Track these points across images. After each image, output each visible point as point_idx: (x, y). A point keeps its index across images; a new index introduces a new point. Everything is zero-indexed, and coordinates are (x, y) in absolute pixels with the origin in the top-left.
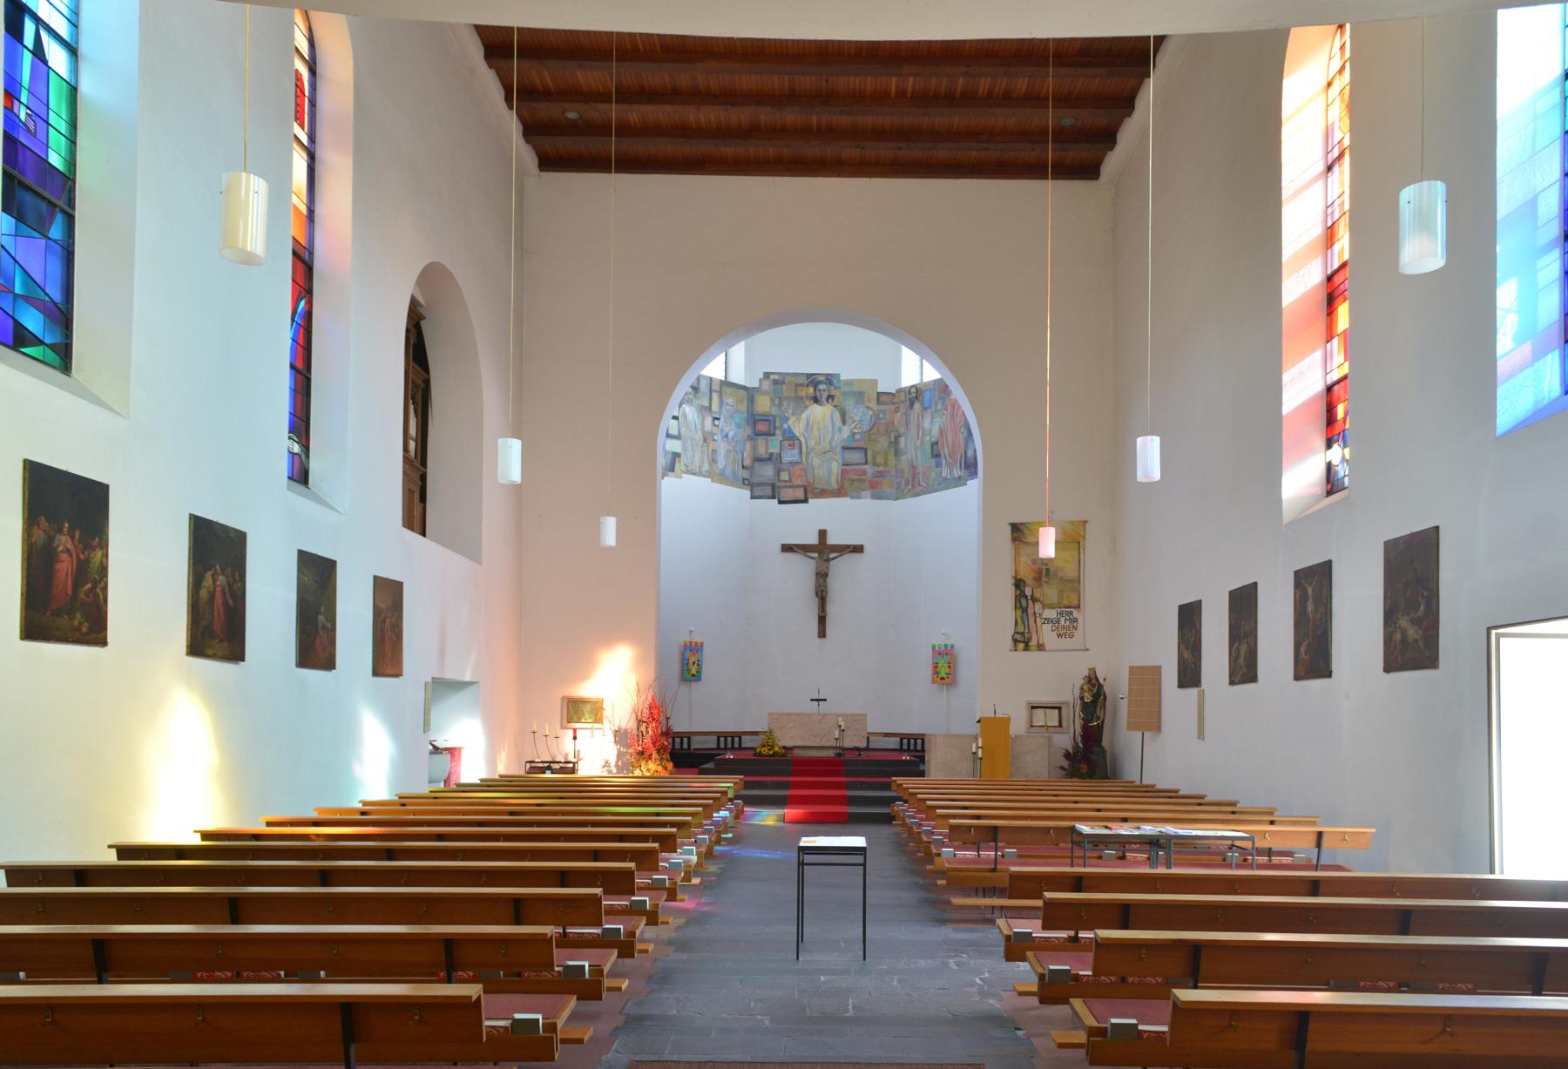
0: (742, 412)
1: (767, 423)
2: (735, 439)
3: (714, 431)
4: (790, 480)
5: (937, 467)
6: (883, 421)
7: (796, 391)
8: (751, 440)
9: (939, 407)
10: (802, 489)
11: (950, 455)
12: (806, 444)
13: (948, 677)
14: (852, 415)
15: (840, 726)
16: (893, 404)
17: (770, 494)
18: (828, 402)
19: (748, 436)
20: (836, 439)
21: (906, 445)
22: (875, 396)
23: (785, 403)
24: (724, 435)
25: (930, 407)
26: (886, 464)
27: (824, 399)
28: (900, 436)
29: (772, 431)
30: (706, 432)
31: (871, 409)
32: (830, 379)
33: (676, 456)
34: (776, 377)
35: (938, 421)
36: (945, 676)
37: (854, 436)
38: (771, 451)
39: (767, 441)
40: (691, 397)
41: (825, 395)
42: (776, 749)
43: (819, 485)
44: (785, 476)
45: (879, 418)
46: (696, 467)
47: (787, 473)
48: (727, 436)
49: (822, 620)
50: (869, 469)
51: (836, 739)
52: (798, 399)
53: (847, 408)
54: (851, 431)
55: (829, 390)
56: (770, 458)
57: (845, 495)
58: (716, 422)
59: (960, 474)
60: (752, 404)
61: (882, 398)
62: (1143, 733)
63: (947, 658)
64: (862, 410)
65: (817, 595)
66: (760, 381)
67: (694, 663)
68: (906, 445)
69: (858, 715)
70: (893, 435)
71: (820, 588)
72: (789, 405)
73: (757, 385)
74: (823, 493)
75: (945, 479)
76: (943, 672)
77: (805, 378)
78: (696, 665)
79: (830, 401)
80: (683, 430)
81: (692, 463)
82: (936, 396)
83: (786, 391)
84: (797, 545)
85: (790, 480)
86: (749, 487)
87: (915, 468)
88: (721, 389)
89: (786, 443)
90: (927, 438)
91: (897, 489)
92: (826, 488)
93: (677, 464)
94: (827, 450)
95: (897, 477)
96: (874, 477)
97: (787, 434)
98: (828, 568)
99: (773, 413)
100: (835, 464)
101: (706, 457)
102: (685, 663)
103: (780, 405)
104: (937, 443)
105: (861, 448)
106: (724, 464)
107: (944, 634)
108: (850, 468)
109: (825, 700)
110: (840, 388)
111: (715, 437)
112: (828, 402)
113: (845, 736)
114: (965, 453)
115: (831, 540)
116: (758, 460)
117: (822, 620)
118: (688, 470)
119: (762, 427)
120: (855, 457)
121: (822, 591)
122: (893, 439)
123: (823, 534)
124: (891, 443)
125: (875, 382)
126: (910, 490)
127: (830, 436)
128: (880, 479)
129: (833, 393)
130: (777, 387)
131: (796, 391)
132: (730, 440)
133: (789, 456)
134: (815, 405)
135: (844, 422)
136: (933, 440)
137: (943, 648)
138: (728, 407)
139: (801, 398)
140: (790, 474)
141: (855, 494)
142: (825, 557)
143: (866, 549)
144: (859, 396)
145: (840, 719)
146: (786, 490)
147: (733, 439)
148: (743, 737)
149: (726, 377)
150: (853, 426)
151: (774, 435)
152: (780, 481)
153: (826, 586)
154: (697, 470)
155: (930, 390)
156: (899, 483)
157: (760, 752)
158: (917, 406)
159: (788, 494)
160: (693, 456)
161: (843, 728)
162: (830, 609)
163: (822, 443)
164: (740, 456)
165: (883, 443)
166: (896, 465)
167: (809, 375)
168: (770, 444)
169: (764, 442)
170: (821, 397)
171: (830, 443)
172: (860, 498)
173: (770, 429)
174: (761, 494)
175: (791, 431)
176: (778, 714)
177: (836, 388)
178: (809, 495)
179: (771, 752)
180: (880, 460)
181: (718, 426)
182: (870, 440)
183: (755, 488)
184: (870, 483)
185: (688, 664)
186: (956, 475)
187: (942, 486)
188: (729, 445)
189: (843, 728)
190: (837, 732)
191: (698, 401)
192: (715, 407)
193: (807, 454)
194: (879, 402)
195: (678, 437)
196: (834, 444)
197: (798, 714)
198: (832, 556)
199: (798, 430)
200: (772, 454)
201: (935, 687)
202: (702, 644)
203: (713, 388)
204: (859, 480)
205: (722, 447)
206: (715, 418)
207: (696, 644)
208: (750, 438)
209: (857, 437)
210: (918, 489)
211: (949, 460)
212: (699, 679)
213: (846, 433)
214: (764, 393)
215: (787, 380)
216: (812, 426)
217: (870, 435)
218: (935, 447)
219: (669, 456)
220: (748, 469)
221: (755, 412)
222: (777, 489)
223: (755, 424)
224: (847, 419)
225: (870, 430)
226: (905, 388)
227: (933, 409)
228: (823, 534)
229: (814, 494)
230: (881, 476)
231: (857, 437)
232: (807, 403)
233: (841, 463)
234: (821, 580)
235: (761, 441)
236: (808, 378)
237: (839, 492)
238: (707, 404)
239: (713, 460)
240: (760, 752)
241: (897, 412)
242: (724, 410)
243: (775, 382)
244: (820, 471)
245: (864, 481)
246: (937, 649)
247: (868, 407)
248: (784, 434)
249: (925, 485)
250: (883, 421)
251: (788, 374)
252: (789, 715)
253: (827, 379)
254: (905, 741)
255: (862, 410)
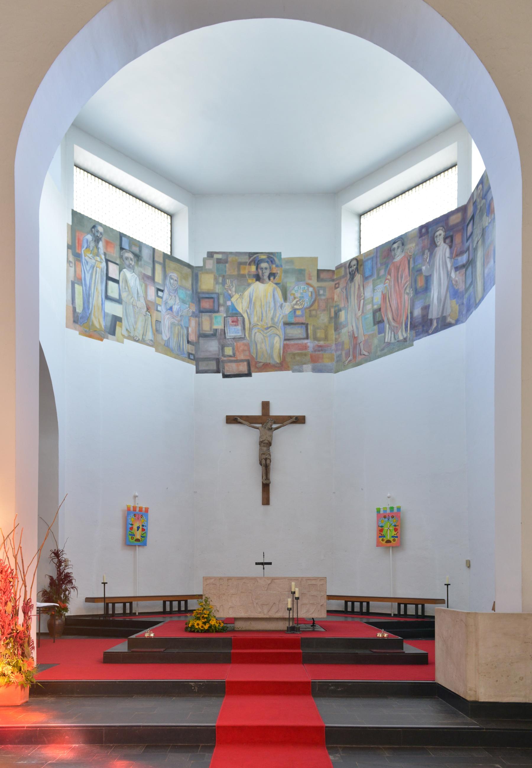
0: (186, 289)
1: (212, 300)
2: (180, 314)
3: (157, 302)
4: (234, 355)
5: (380, 333)
6: (323, 297)
7: (239, 270)
8: (196, 317)
9: (382, 272)
10: (246, 363)
11: (393, 319)
12: (249, 319)
13: (394, 540)
14: (293, 292)
15: (294, 593)
16: (333, 280)
17: (215, 368)
18: (269, 279)
19: (193, 313)
20: (278, 315)
21: (346, 318)
22: (315, 273)
23: (228, 281)
24: (168, 307)
25: (371, 276)
26: (326, 338)
27: (266, 277)
28: (340, 310)
29: (216, 309)
30: (149, 301)
31: (312, 286)
32: (271, 257)
33: (116, 320)
34: (220, 256)
35: (380, 288)
36: (392, 539)
37: (295, 312)
38: (215, 327)
39: (211, 319)
40: (133, 263)
41: (267, 274)
42: (213, 622)
43: (262, 360)
44: (228, 351)
45: (320, 295)
46: (139, 333)
47: (231, 348)
48: (171, 309)
49: (266, 487)
50: (310, 343)
51: (289, 609)
52: (241, 277)
53: (288, 285)
54: (293, 307)
55: (270, 268)
56: (214, 334)
57: (287, 369)
58: (160, 293)
59: (405, 335)
60: (197, 282)
61: (322, 276)
62: (264, 576)
63: (394, 521)
64: (302, 287)
65: (261, 464)
66: (204, 260)
67: (138, 528)
68: (346, 318)
69: (316, 579)
70: (333, 311)
71: (264, 456)
72: (232, 282)
73: (201, 264)
74: (266, 367)
75: (389, 344)
76: (389, 534)
77: (247, 257)
78: (140, 529)
79: (272, 278)
80: (124, 295)
81: (134, 330)
82: (378, 263)
83: (230, 269)
84: (241, 417)
85: (234, 355)
86: (194, 362)
87: (355, 338)
88: (164, 261)
89: (230, 320)
90: (369, 307)
91: (337, 361)
92: (268, 362)
93: (118, 329)
94: (269, 326)
95: (337, 350)
96: (315, 351)
97: (230, 311)
98: (271, 436)
99: (217, 291)
100: (277, 339)
101: (150, 326)
102: (129, 529)
103: (224, 283)
104: (380, 310)
105: (302, 324)
106: (168, 336)
107: (389, 497)
108: (292, 342)
109: (270, 564)
110: (281, 266)
111: (159, 308)
112: (269, 279)
113: (299, 605)
114: (412, 313)
115: (274, 412)
116: (203, 336)
117: (266, 487)
118: (129, 336)
119: (206, 304)
120: (297, 332)
121: (266, 459)
122: (333, 314)
123: (266, 405)
124: (331, 318)
125: (314, 260)
126: (350, 361)
127: (272, 312)
128: (321, 353)
129: (274, 272)
130: (221, 266)
131: (239, 270)
132: (175, 314)
133: (233, 332)
134: (258, 282)
135: (285, 299)
136: (376, 307)
137: (388, 511)
138: (172, 281)
139: (243, 276)
140: (233, 349)
141: (296, 367)
142: (268, 426)
143: (307, 420)
144: (300, 274)
145: (293, 584)
146: (229, 364)
147: (178, 312)
148: (189, 601)
149: (171, 252)
150: (294, 302)
151: (218, 312)
152: (224, 355)
153: (270, 455)
154: (141, 338)
155: (372, 258)
156: (339, 356)
157: (193, 626)
158: (358, 278)
159: (231, 368)
160: (136, 323)
161: (297, 595)
162: (275, 478)
163: (264, 318)
164: (185, 331)
165: (324, 318)
166: (336, 339)
167: (251, 254)
168: (214, 321)
169: (208, 318)
170: (263, 275)
171: (272, 319)
172: (300, 371)
173: (214, 306)
174: (207, 368)
175: (234, 308)
176: (215, 578)
177: (277, 266)
178: (252, 369)
179: (206, 627)
180: (320, 334)
181: (161, 298)
182: (311, 316)
183: (200, 363)
184: (311, 357)
185: (131, 529)
186: (401, 338)
187: (385, 351)
188: (173, 318)
189: (297, 595)
190: (290, 600)
191: (140, 269)
192: (159, 277)
193: (250, 330)
194: (319, 279)
195: (119, 301)
196: (276, 320)
197: (241, 578)
198: (274, 426)
199: (241, 306)
200: (216, 330)
201: (379, 550)
202: (147, 510)
203: (156, 259)
204: (299, 355)
205: (167, 321)
206: (158, 290)
207: (141, 509)
208: (194, 315)
209: (299, 313)
210: (359, 358)
211: (393, 323)
212: (144, 544)
213: (287, 309)
214: (208, 272)
215: (229, 260)
216: (254, 303)
217: (310, 311)
218: (378, 314)
219: (109, 319)
220: (193, 345)
221: (199, 290)
222: (221, 364)
223: (199, 301)
224: (289, 295)
225: (311, 306)
226: (345, 263)
227: (375, 277)
228: (266, 405)
229: (256, 367)
230: (322, 350)
231: (299, 313)
232: (250, 281)
233: (282, 337)
234: (265, 449)
235: (205, 318)
236: (250, 257)
237: (282, 366)
238: (149, 273)
239: (157, 330)
240: (193, 626)
241: (336, 288)
242: (167, 282)
243: (219, 261)
244: (263, 345)
245: (305, 355)
246: (382, 512)
247: (309, 285)
248: (227, 310)
249: (366, 353)
250: (323, 297)
251: (231, 253)
252: (229, 579)
253: (269, 257)
254: (350, 604)
255: (302, 287)
